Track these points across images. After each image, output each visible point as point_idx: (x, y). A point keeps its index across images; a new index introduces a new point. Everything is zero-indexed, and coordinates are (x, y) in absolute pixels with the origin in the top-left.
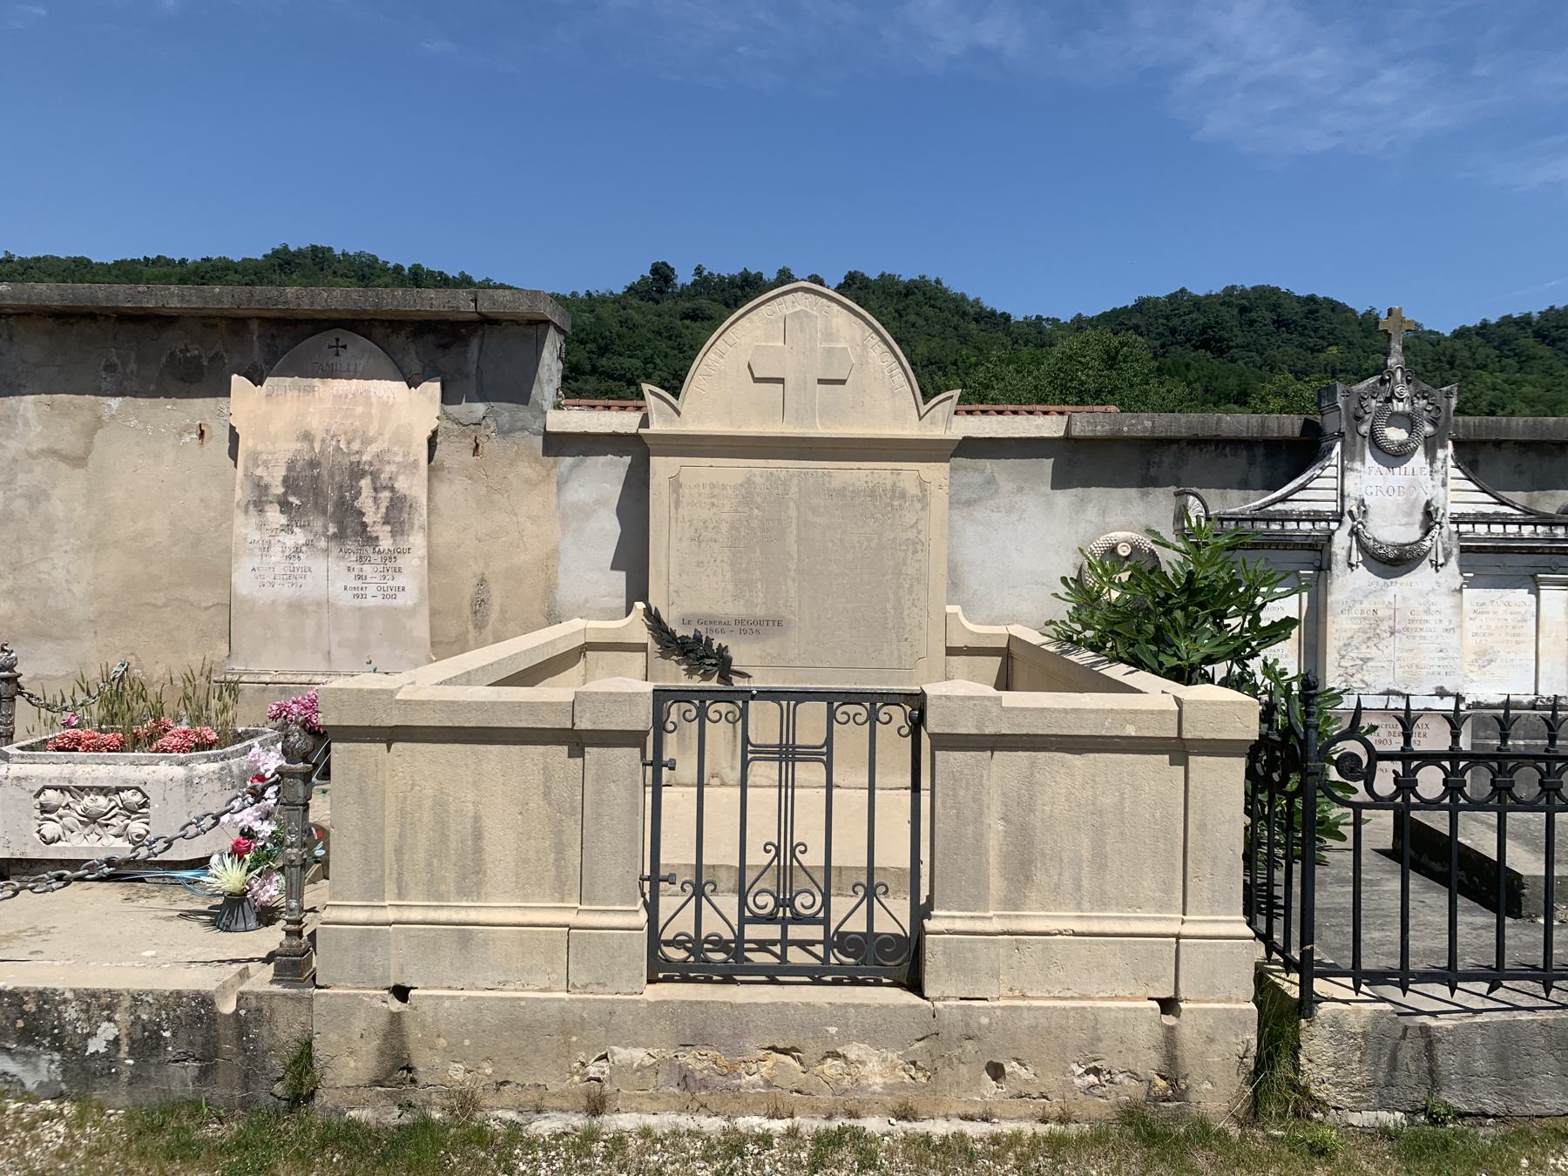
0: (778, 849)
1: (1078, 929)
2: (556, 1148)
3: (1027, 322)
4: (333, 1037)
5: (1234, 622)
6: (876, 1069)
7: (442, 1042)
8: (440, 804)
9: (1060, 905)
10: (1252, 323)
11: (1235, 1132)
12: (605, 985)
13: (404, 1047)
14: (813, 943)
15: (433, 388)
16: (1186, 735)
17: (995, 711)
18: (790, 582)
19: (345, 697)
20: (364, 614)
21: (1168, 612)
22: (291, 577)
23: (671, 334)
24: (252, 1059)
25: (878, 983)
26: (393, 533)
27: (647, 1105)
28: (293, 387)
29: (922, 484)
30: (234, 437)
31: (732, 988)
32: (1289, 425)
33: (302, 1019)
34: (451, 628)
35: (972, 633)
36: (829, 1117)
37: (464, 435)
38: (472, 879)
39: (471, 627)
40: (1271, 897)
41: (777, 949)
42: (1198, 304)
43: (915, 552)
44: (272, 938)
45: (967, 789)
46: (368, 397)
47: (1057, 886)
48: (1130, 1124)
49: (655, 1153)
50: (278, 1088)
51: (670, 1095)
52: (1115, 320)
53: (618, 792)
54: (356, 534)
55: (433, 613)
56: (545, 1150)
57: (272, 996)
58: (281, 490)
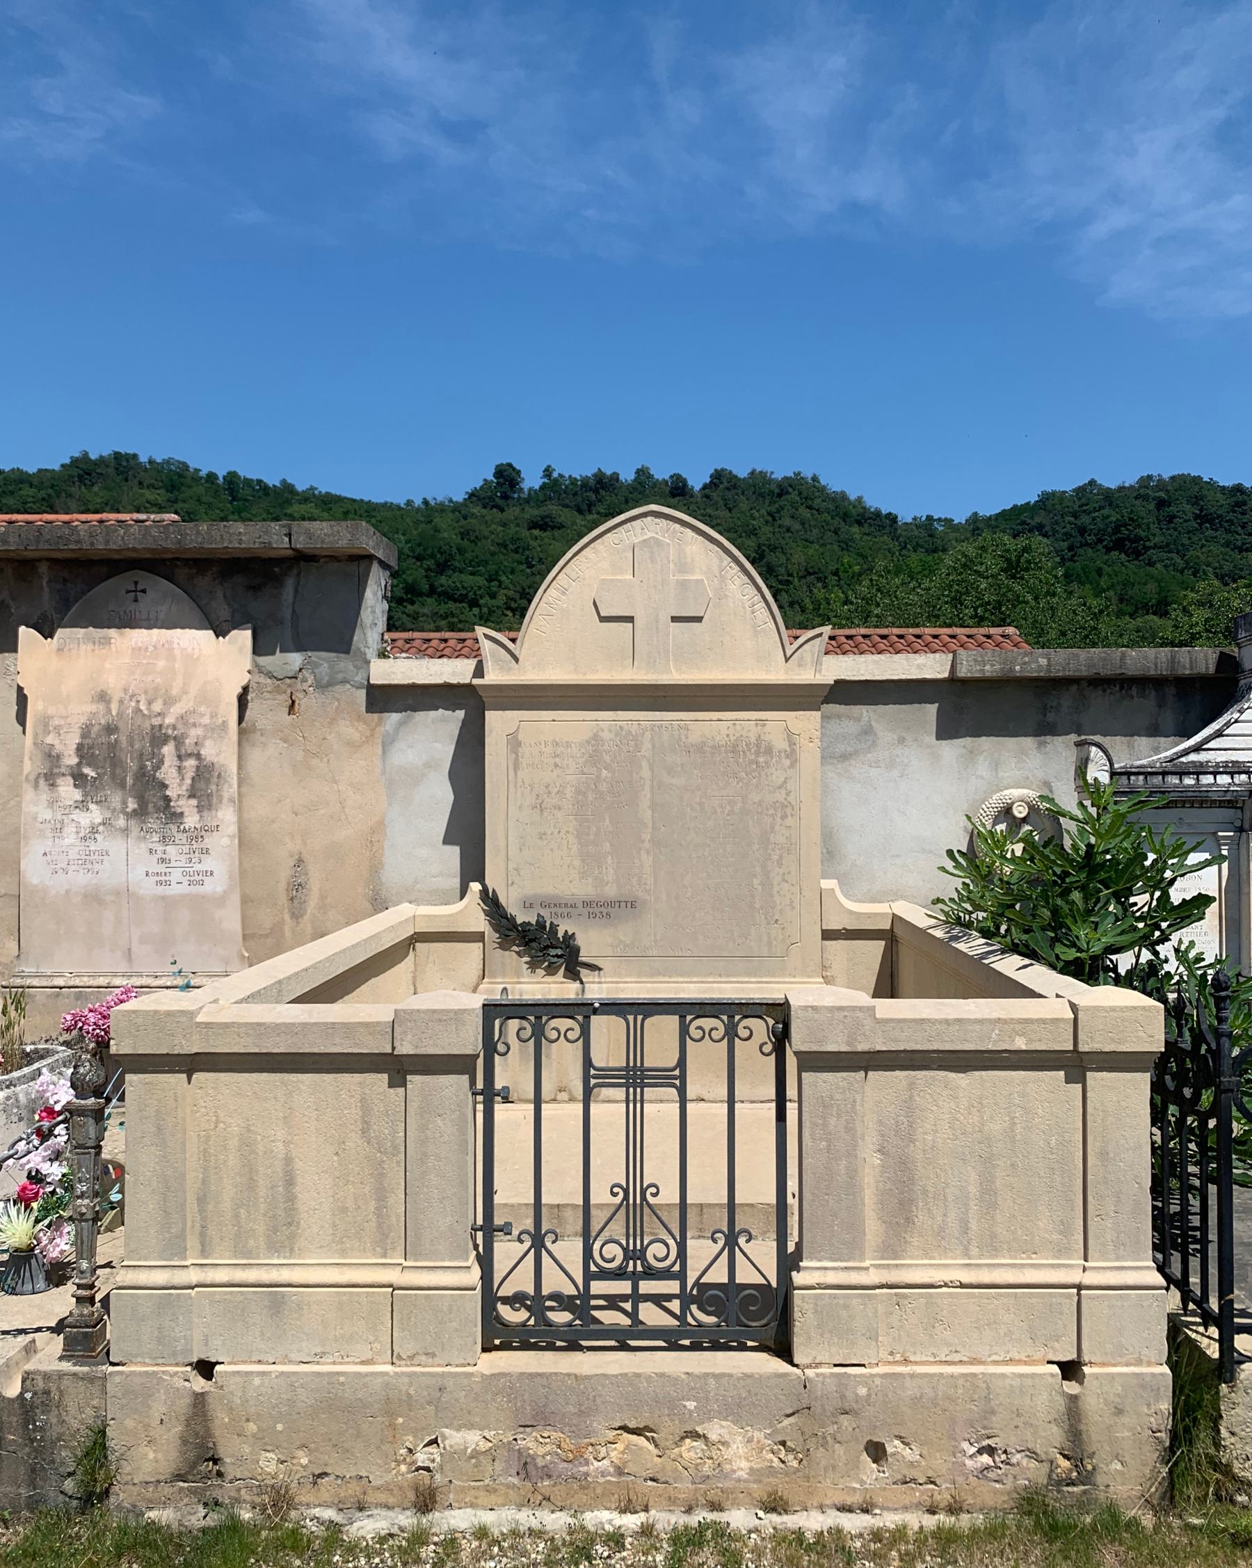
0: (626, 1191)
1: (965, 1280)
2: (380, 1554)
3: (917, 524)
4: (129, 1423)
5: (1141, 900)
6: (741, 1451)
7: (252, 1427)
8: (246, 1144)
9: (945, 1252)
10: (1171, 519)
11: (1148, 1521)
12: (433, 1355)
13: (208, 1434)
14: (669, 1297)
15: (243, 638)
16: (1083, 1048)
17: (868, 1023)
18: (644, 856)
19: (140, 1021)
20: (169, 903)
21: (1065, 893)
22: (86, 862)
23: (519, 547)
24: (38, 1451)
25: (742, 1348)
26: (200, 808)
27: (484, 1499)
28: (88, 639)
29: (790, 736)
30: (22, 699)
31: (577, 1356)
32: (1201, 659)
33: (95, 1402)
34: (266, 918)
35: (851, 912)
36: (689, 1510)
37: (277, 690)
38: (283, 1234)
39: (287, 917)
40: (1185, 1228)
41: (628, 1306)
42: (1109, 497)
43: (784, 817)
44: (60, 1302)
45: (839, 1116)
46: (171, 650)
47: (942, 1229)
48: (1029, 1513)
49: (492, 1558)
50: (69, 1485)
51: (508, 1486)
52: (1016, 520)
53: (445, 1128)
54: (158, 810)
55: (245, 900)
56: (368, 1557)
57: (61, 1375)
58: (75, 760)
